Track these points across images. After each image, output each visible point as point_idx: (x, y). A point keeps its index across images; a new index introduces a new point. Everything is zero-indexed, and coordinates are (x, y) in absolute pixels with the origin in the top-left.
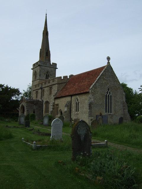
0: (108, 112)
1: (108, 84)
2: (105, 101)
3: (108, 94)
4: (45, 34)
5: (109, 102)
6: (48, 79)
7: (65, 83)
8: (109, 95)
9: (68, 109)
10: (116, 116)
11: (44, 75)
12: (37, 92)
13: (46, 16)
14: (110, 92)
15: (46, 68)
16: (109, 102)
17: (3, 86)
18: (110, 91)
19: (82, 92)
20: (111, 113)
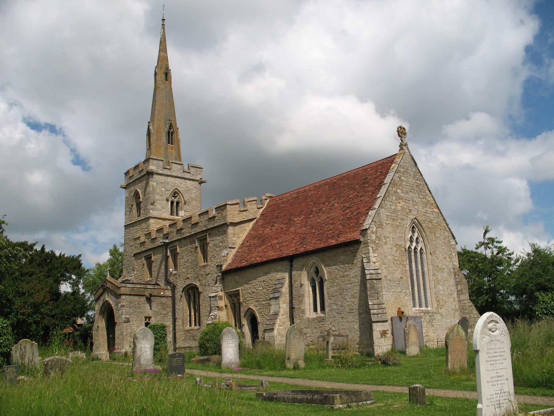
0: (420, 306)
1: (410, 211)
2: (408, 268)
3: (414, 244)
4: (161, 77)
5: (417, 271)
6: (177, 215)
7: (252, 224)
8: (415, 248)
9: (11, 362)
10: (442, 315)
11: (165, 202)
12: (148, 258)
13: (163, 25)
14: (417, 239)
15: (169, 179)
16: (417, 271)
17: (32, 247)
18: (416, 235)
19: (333, 242)
20: (427, 306)
